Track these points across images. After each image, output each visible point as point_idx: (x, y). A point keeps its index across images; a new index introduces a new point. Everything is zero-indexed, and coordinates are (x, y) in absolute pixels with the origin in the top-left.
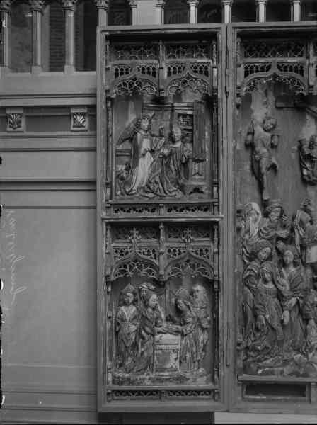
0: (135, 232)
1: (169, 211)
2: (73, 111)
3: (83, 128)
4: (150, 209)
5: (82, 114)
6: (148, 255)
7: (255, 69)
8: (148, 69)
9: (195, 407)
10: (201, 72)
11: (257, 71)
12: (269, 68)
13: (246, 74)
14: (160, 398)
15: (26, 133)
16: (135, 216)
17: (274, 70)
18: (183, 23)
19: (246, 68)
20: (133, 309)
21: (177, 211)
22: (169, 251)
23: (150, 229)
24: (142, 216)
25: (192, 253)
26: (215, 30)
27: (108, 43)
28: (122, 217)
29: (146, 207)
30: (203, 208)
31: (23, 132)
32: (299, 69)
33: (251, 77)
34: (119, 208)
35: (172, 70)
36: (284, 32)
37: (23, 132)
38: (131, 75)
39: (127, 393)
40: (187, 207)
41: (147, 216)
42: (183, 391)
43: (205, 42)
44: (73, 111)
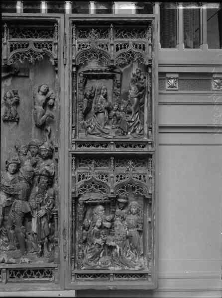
0: (131, 163)
1: (80, 146)
2: (168, 76)
3: (175, 88)
4: (141, 146)
5: (174, 78)
6: (140, 179)
7: (17, 47)
8: (140, 46)
9: (105, 286)
10: (140, 48)
11: (19, 48)
12: (27, 45)
13: (12, 50)
14: (109, 279)
15: (179, 92)
16: (129, 150)
17: (31, 46)
18: (149, 13)
19: (12, 45)
20: (135, 217)
21: (140, 147)
22: (117, 176)
23: (102, 159)
24: (145, 149)
25: (96, 178)
26: (151, 19)
27: (74, 26)
28: (84, 150)
29: (101, 144)
30: (86, 145)
31: (177, 90)
32: (142, 47)
33: (15, 52)
34: (81, 144)
35: (119, 47)
36: (94, 21)
37: (177, 90)
38: (128, 50)
39: (85, 276)
40: (92, 144)
41: (101, 150)
42: (130, 275)
43: (47, 28)
44: (168, 76)
